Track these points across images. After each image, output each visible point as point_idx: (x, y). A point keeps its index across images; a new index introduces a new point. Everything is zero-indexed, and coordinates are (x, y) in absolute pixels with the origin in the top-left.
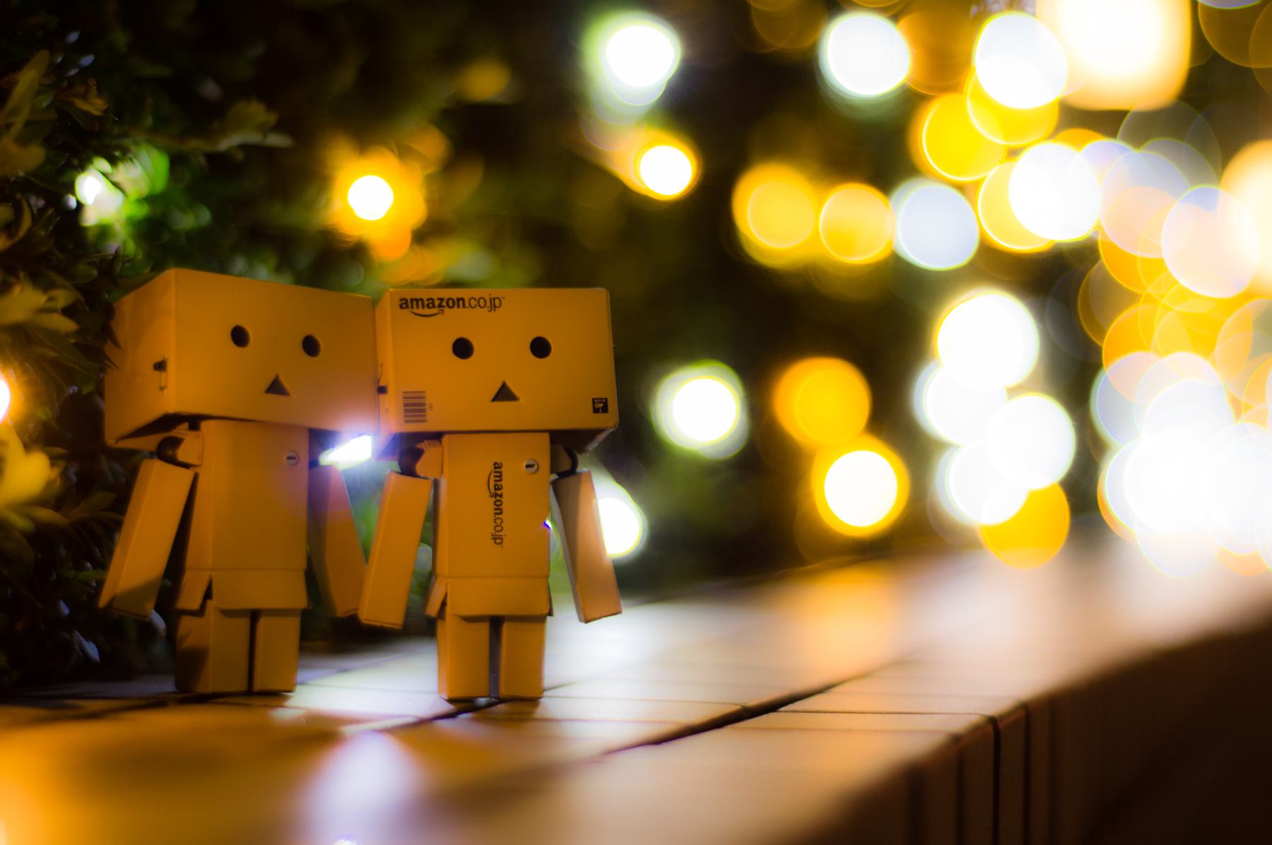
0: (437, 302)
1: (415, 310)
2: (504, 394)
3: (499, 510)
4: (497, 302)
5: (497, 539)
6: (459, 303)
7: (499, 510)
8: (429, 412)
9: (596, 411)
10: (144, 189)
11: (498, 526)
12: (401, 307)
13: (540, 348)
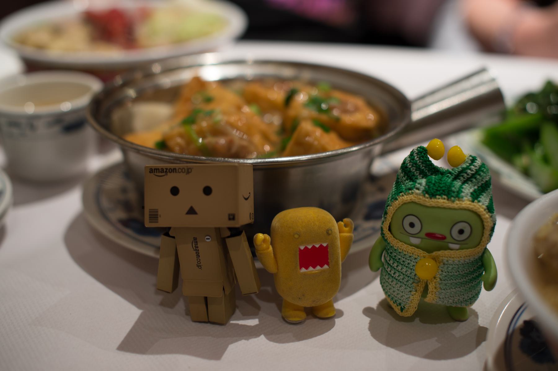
0: (165, 170)
1: (156, 174)
2: (192, 211)
3: (198, 255)
4: (190, 170)
5: (199, 266)
6: (174, 170)
7: (198, 255)
8: (159, 218)
9: (230, 219)
10: (487, 205)
11: (199, 261)
12: (150, 172)
13: (207, 191)
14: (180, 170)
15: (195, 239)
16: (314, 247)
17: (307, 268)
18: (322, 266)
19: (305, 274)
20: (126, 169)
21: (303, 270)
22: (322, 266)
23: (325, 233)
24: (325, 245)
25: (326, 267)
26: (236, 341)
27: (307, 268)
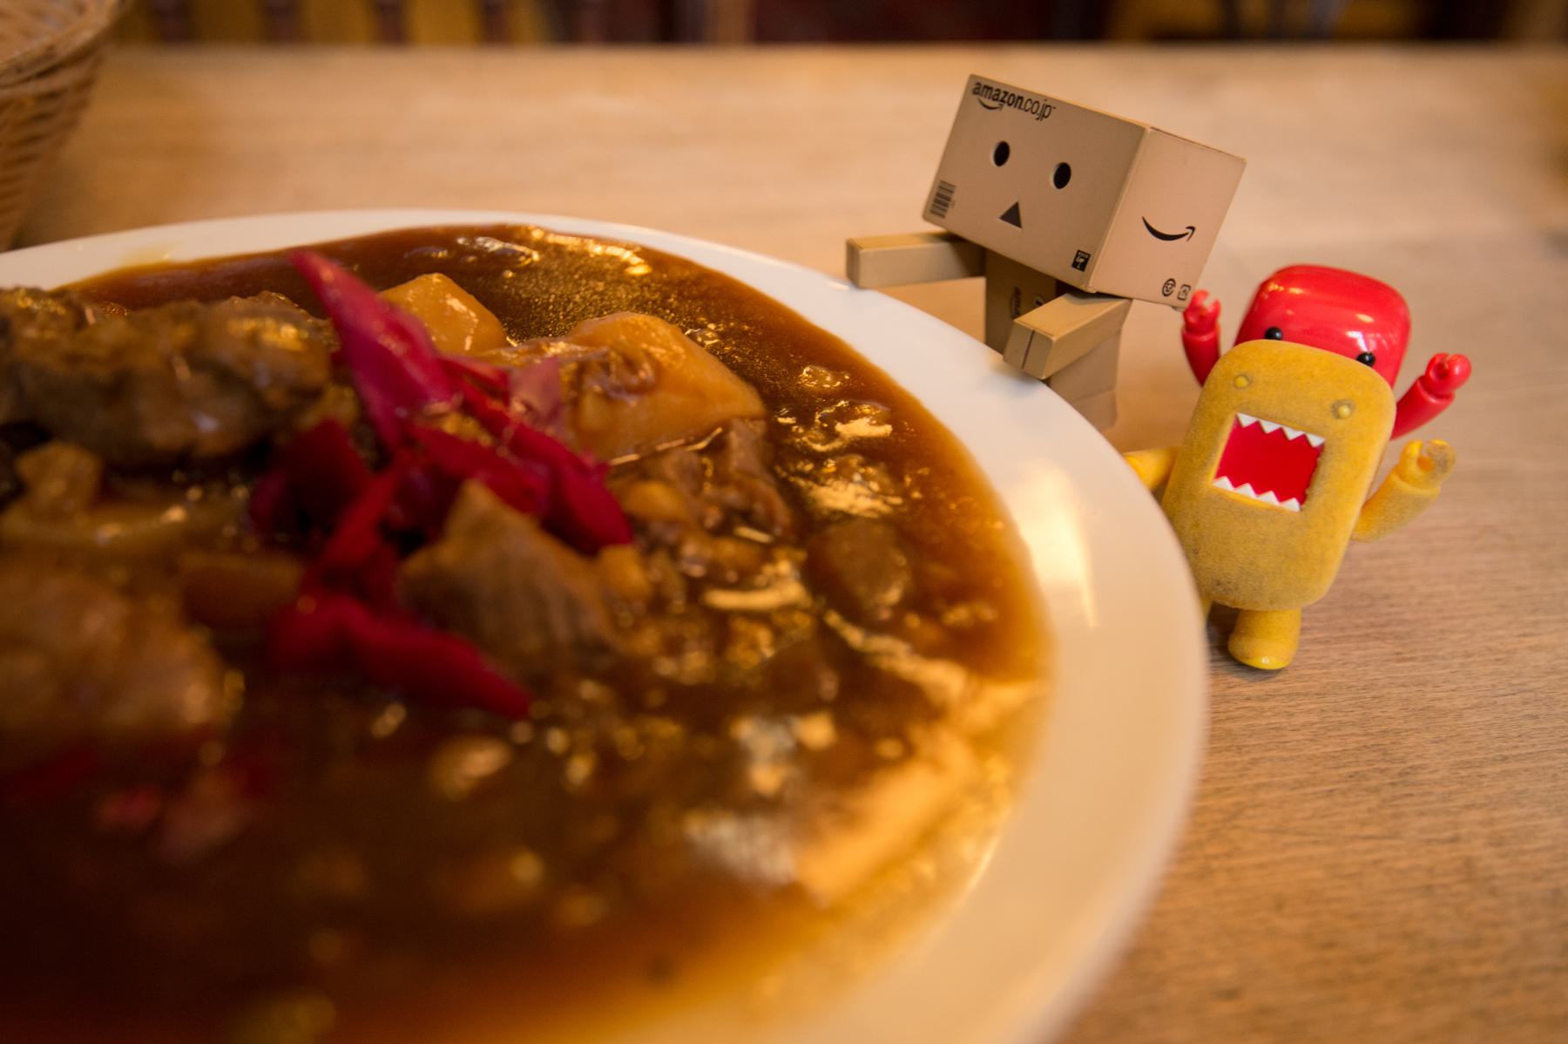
8: (950, 210)
9: (1075, 265)
14: (1029, 106)
15: (1018, 292)
16: (1280, 432)
17: (1236, 484)
18: (1282, 497)
19: (1221, 495)
20: (509, 333)
21: (1225, 483)
22: (1282, 497)
23: (1328, 404)
24: (1315, 441)
25: (1293, 504)
26: (902, 392)
27: (1236, 484)
